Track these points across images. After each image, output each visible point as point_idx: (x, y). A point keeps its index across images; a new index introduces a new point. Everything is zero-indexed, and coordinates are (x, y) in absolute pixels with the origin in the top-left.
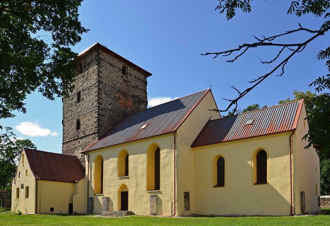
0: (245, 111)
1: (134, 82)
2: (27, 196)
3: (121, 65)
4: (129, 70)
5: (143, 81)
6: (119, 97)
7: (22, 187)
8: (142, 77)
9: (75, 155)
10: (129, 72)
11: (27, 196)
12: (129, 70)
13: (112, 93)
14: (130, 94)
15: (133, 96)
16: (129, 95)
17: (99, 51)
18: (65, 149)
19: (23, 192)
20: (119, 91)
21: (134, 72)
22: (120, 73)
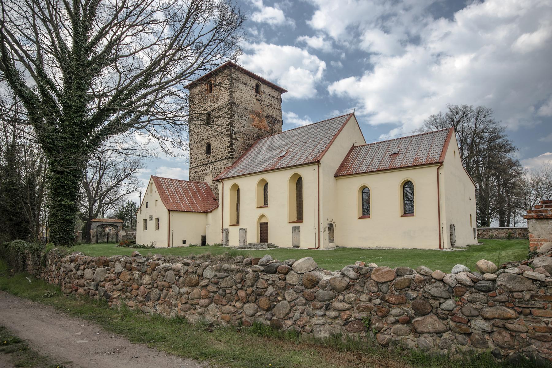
0: (296, 230)
1: (268, 101)
2: (158, 227)
3: (253, 83)
4: (263, 88)
5: (277, 99)
6: (253, 119)
7: (151, 218)
8: (276, 94)
9: (205, 181)
10: (262, 90)
11: (158, 227)
12: (263, 88)
13: (245, 114)
14: (264, 113)
15: (268, 116)
16: (263, 115)
17: (231, 70)
18: (193, 176)
19: (151, 224)
20: (253, 112)
21: (267, 90)
22: (254, 92)
